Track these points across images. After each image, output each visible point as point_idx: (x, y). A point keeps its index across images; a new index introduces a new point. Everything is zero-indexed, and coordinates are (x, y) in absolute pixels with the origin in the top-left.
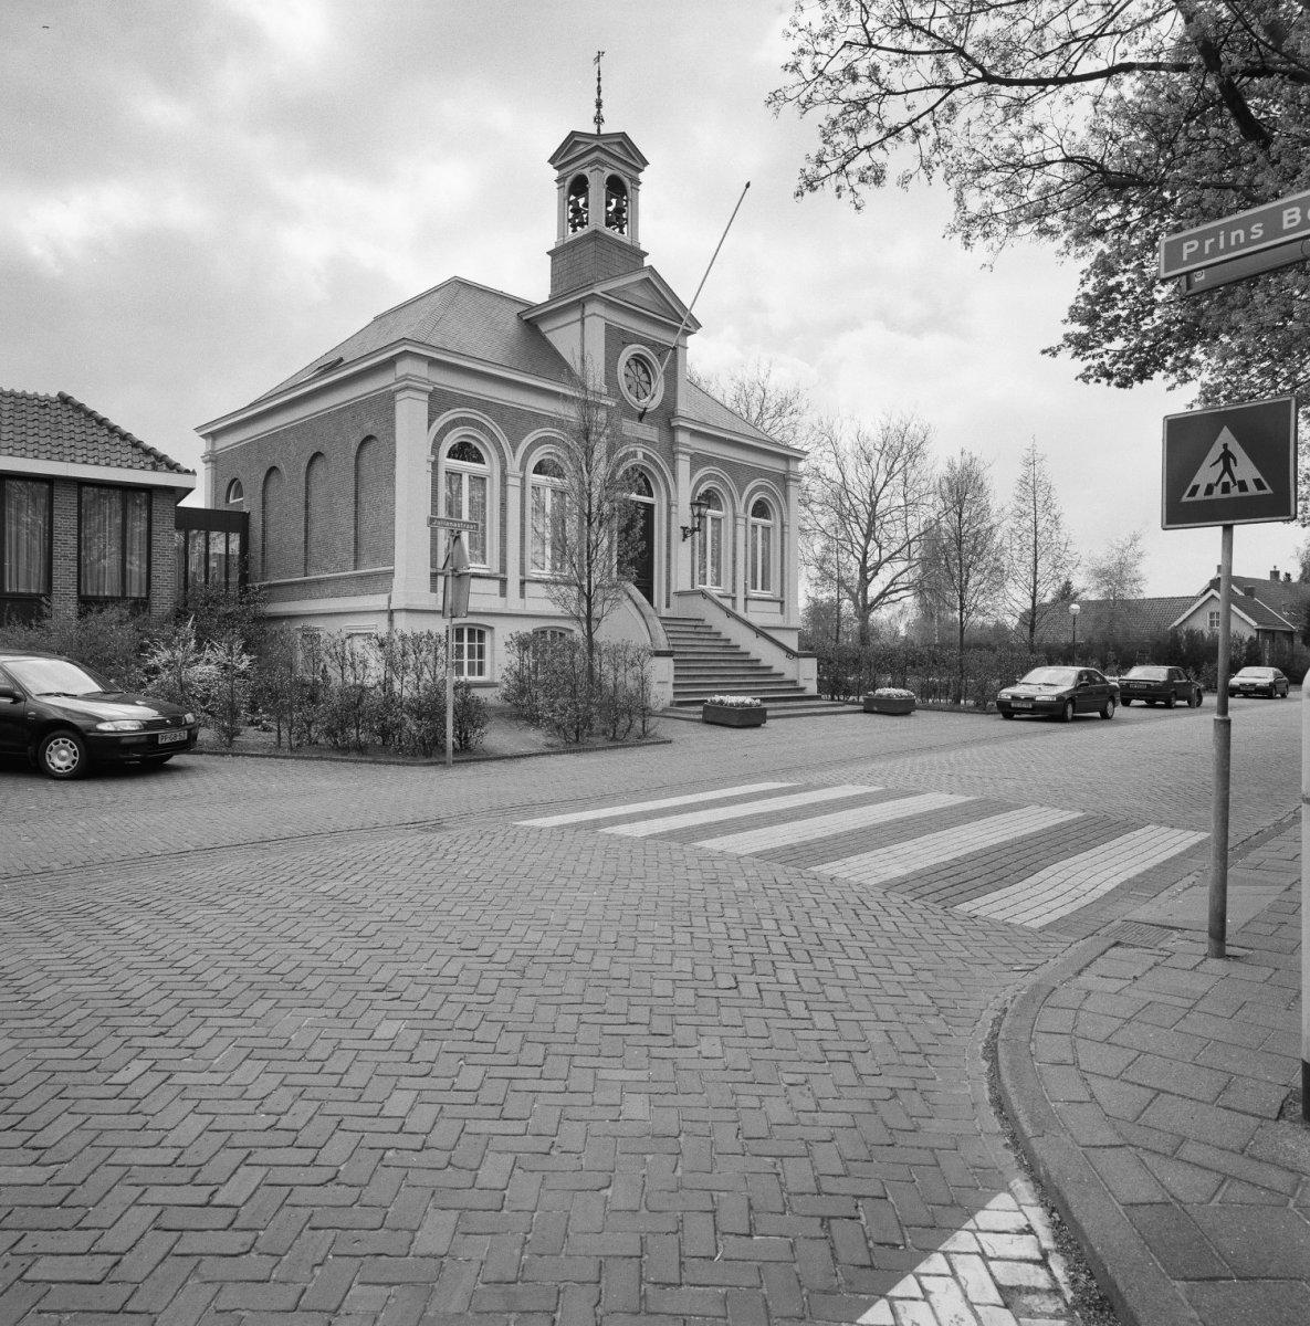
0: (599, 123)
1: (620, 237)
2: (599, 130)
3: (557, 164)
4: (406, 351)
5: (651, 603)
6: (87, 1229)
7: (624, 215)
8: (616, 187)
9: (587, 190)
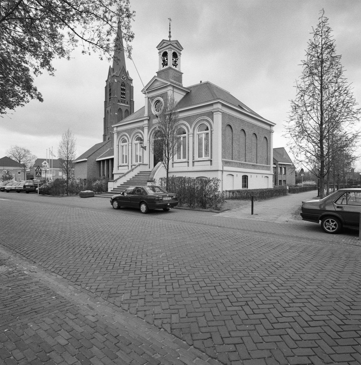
0: (170, 37)
1: (176, 69)
2: (170, 39)
3: (159, 48)
4: (219, 102)
5: (155, 165)
6: (342, 329)
7: (177, 63)
8: (175, 55)
9: (167, 55)
